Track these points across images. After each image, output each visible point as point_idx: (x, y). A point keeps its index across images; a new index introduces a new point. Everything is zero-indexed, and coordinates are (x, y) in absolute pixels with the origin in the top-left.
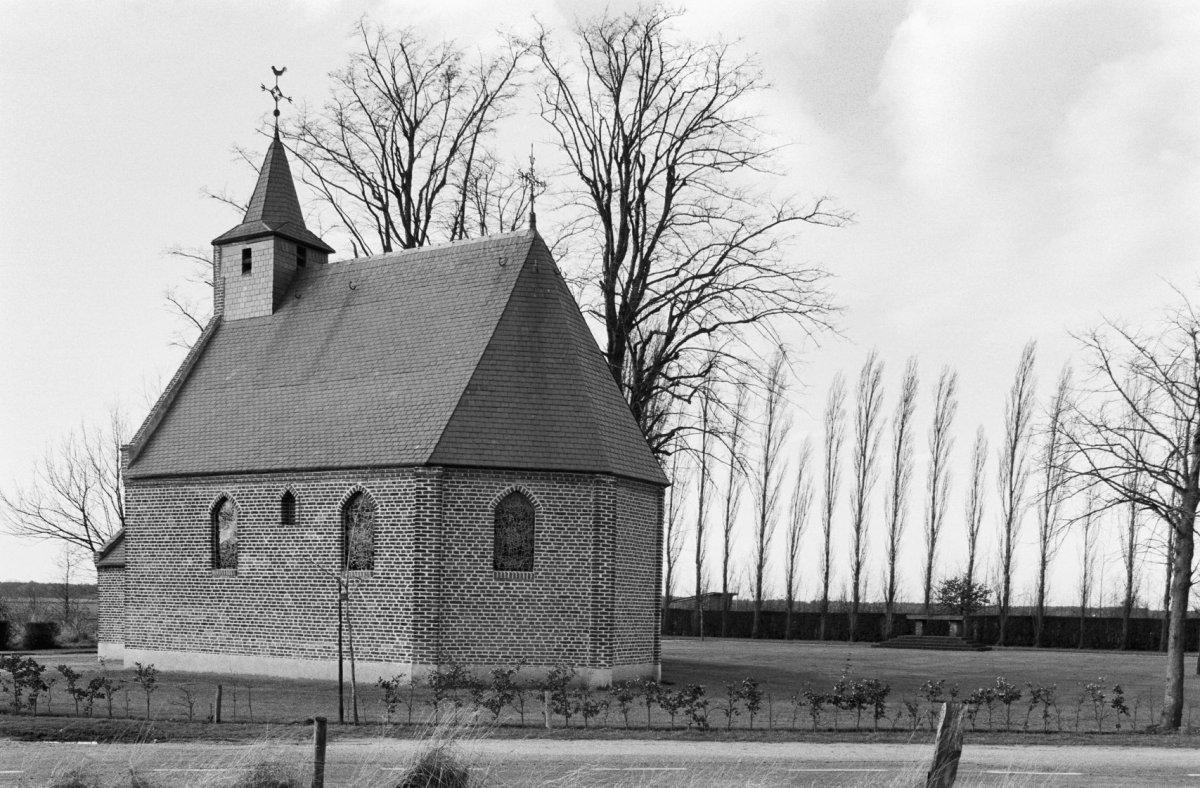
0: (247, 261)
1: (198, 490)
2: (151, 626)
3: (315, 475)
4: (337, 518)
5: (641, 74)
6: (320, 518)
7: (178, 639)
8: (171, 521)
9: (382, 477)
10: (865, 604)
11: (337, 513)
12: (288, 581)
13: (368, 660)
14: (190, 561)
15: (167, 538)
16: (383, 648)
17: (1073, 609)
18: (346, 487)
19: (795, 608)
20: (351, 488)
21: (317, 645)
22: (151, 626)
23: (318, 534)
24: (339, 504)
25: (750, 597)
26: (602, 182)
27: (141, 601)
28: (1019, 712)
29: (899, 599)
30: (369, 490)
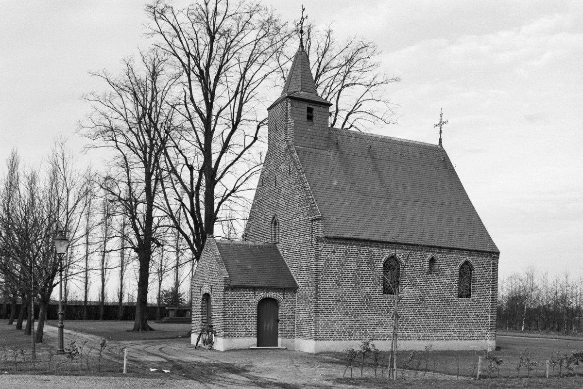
0: (310, 114)
1: (375, 250)
2: (337, 327)
3: (457, 252)
4: (457, 273)
5: (282, 76)
6: (449, 272)
7: (358, 334)
8: (354, 266)
9: (478, 256)
10: (90, 302)
11: (457, 270)
12: (430, 302)
13: (468, 340)
14: (368, 290)
15: (351, 275)
16: (476, 334)
17: (96, 302)
18: (387, 253)
19: (104, 304)
20: (464, 259)
21: (444, 334)
22: (337, 327)
23: (447, 280)
24: (458, 266)
25: (81, 298)
26: (201, 114)
27: (329, 312)
28: (512, 343)
29: (89, 300)
30: (472, 261)
